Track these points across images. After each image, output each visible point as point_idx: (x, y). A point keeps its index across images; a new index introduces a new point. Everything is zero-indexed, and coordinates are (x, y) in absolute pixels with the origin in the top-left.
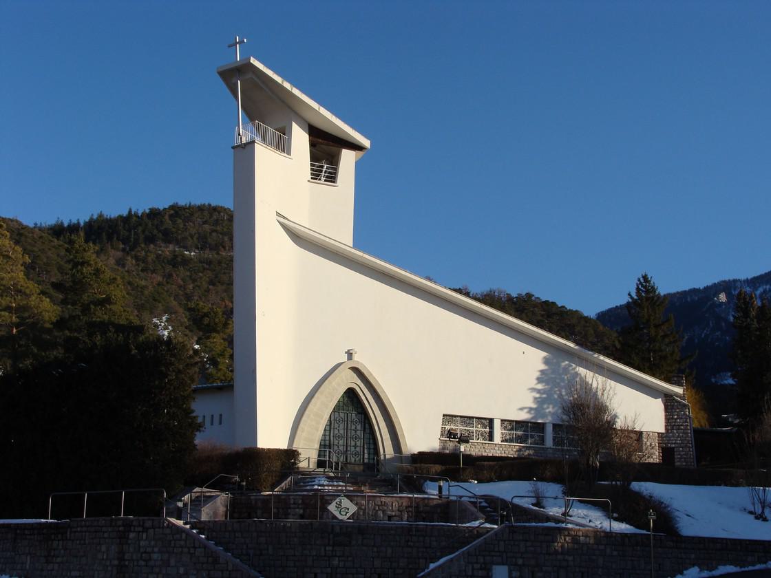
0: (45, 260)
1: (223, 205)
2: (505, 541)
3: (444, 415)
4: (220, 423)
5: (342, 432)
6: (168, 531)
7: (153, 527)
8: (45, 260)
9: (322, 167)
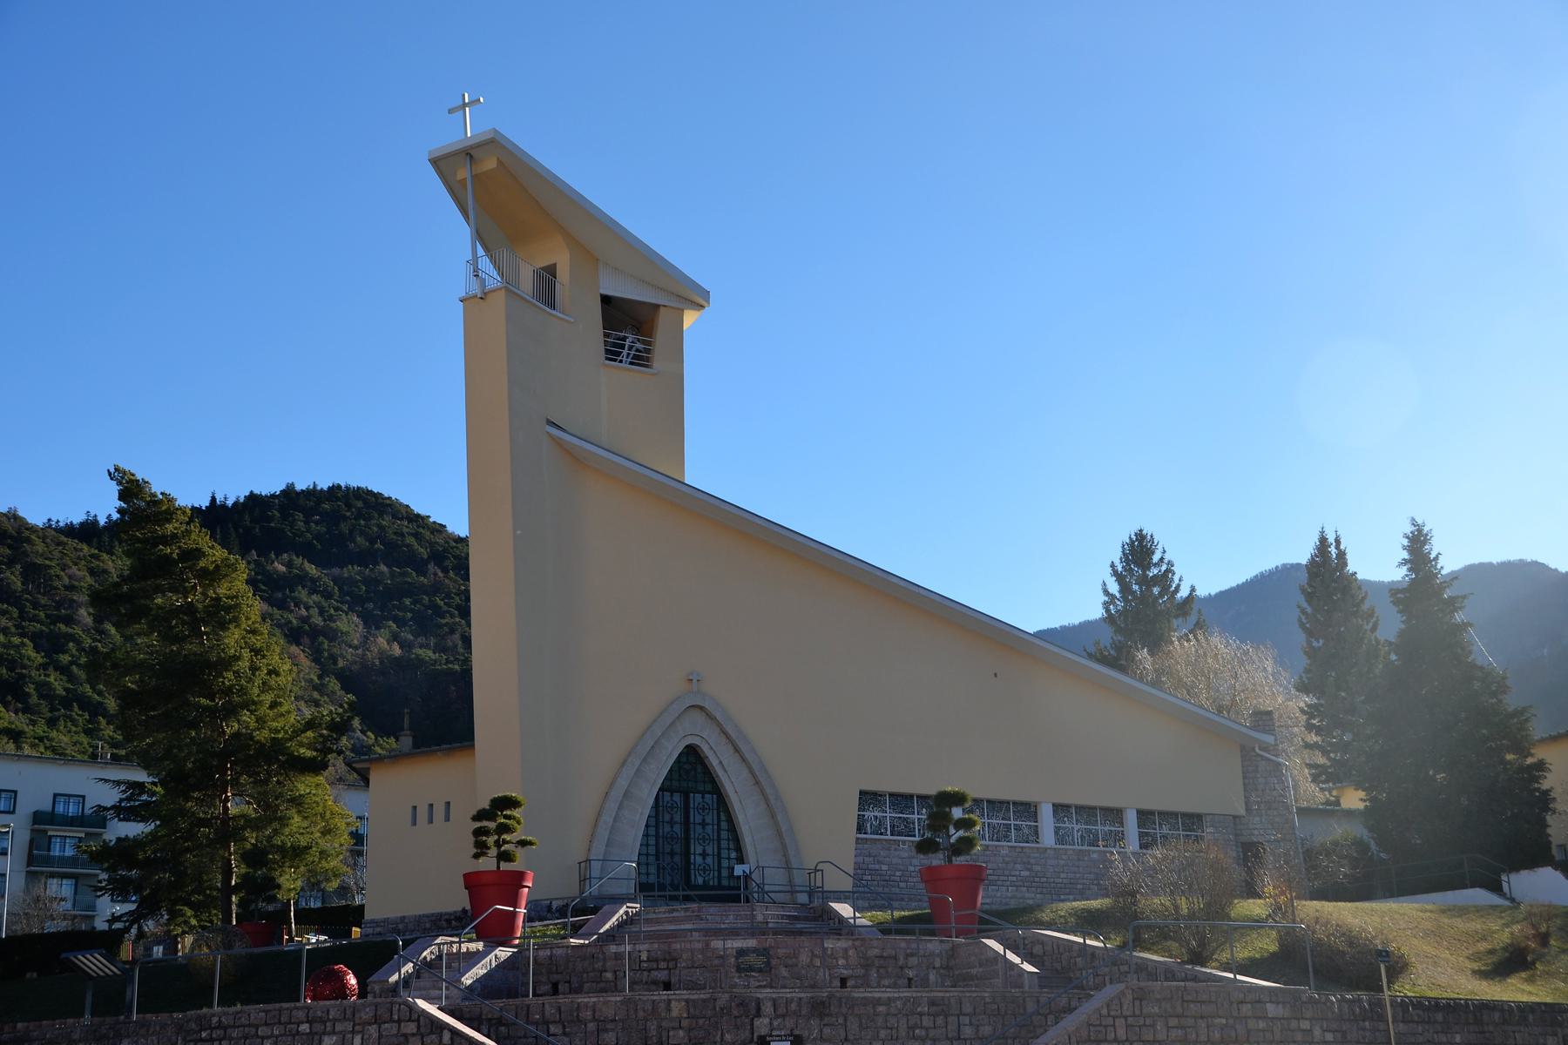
0: (67, 581)
1: (363, 485)
2: (1126, 1018)
3: (868, 798)
4: (447, 819)
5: (677, 828)
6: (411, 1028)
7: (377, 1020)
8: (67, 581)
9: (624, 339)
